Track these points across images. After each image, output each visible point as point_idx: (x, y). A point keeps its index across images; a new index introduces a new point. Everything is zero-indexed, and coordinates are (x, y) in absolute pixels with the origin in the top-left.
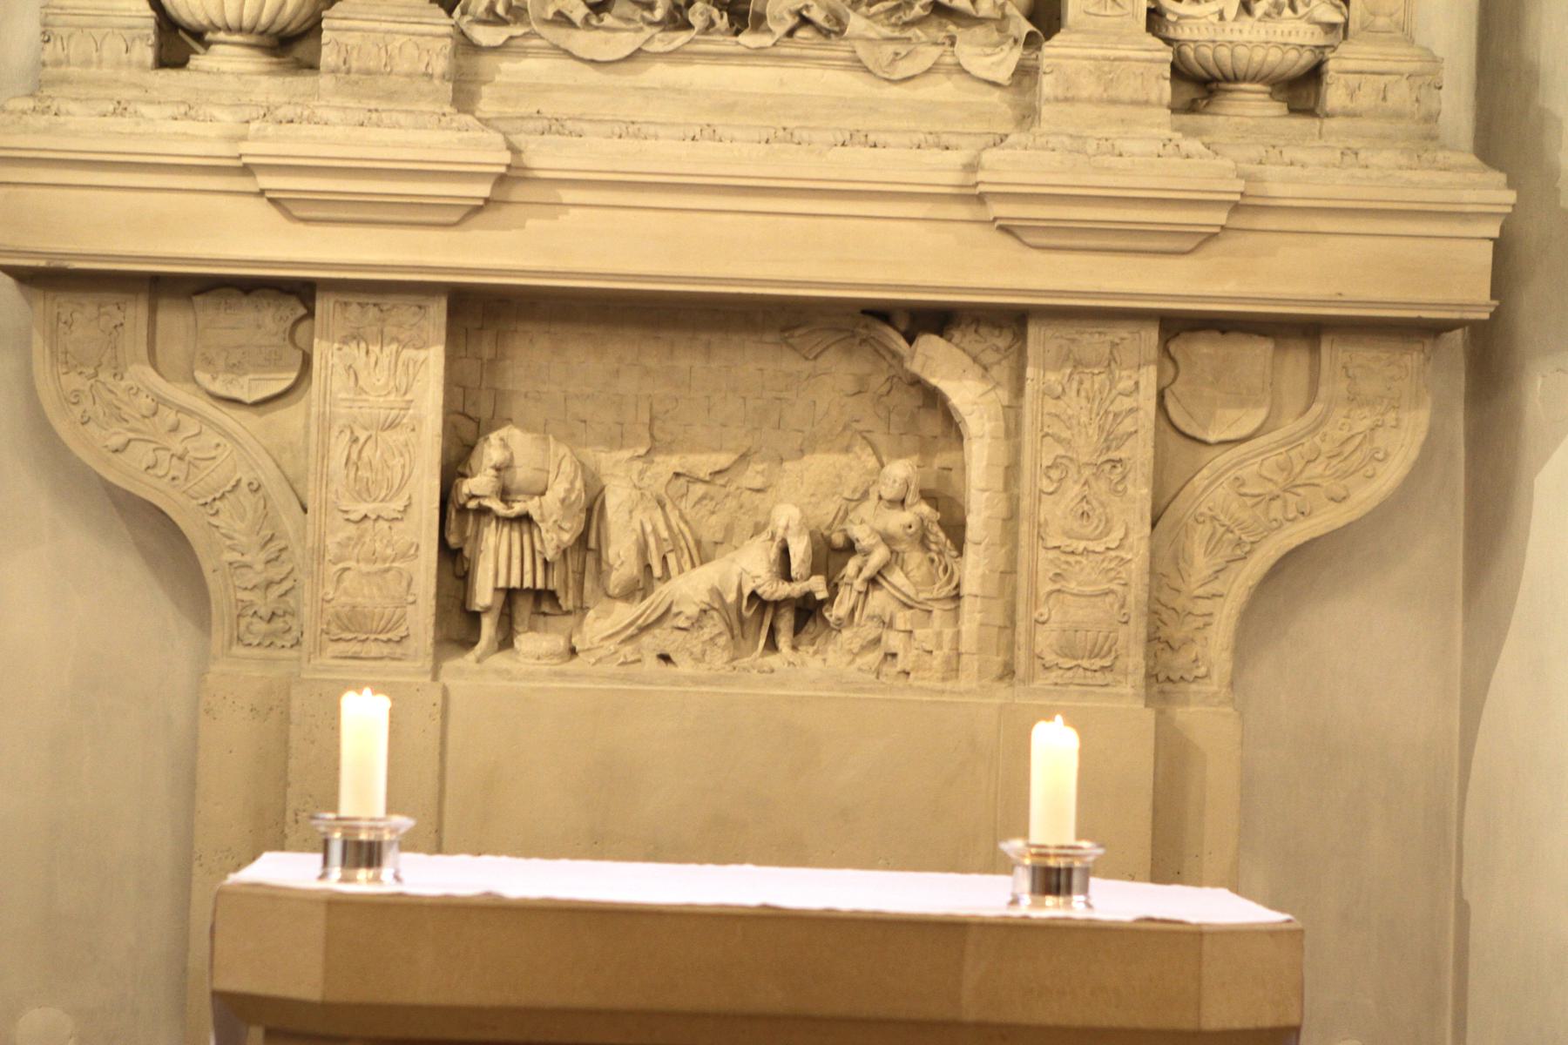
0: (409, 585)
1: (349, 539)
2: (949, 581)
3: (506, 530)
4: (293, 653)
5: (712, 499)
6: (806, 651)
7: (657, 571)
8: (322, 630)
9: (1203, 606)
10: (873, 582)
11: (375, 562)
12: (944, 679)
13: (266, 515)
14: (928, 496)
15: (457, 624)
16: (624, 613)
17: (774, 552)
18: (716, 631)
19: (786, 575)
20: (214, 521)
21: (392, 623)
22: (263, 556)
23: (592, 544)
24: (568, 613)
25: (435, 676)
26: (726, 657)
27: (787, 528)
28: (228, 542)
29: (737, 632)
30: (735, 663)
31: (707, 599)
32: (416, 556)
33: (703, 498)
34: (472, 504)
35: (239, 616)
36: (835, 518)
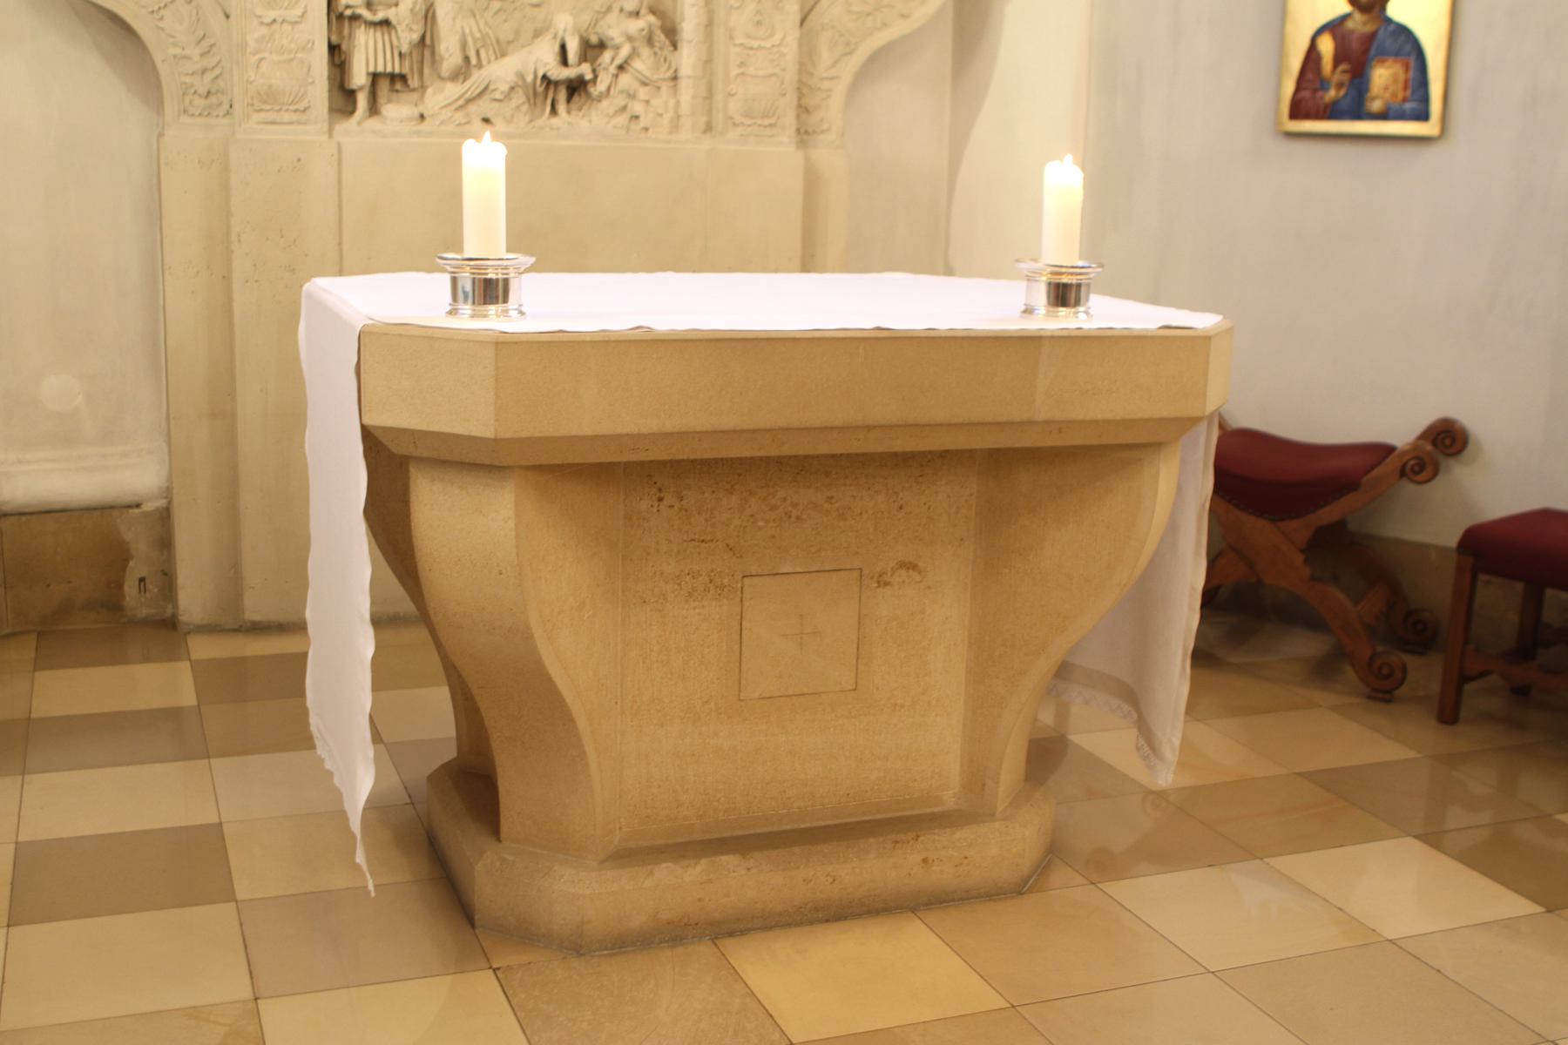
0: (309, 70)
1: (264, 37)
2: (669, 68)
3: (379, 35)
4: (226, 121)
5: (505, 11)
6: (576, 117)
7: (474, 61)
8: (248, 105)
9: (825, 85)
10: (621, 68)
11: (283, 53)
12: (670, 133)
13: (199, 20)
14: (653, 11)
15: (340, 100)
16: (453, 90)
17: (557, 48)
18: (520, 102)
19: (564, 61)
20: (161, 24)
21: (298, 97)
22: (198, 51)
23: (428, 41)
24: (414, 90)
25: (330, 135)
26: (527, 118)
27: (565, 30)
28: (171, 40)
29: (532, 101)
30: (533, 123)
31: (515, 79)
32: (312, 48)
33: (499, 10)
34: (348, 12)
35: (184, 94)
36: (590, 24)
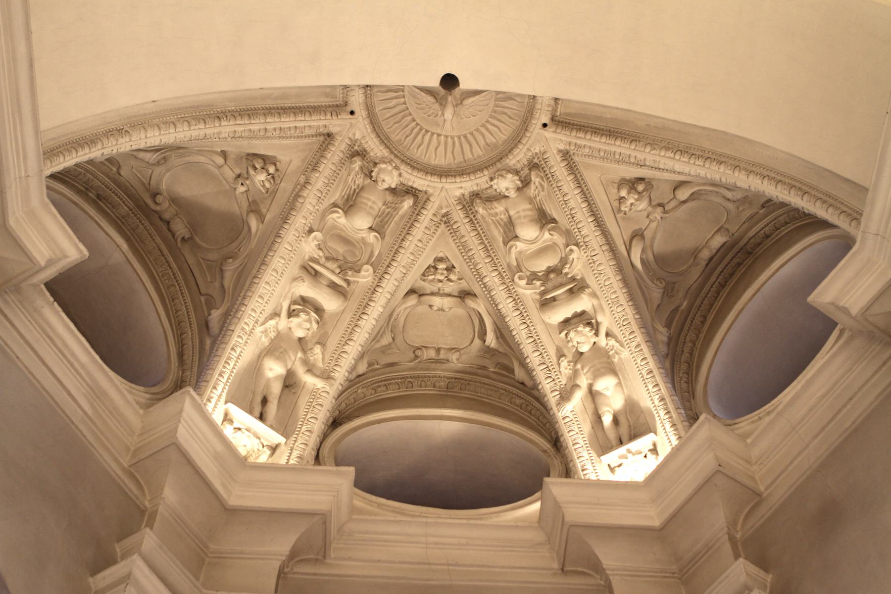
27: (507, 189)
